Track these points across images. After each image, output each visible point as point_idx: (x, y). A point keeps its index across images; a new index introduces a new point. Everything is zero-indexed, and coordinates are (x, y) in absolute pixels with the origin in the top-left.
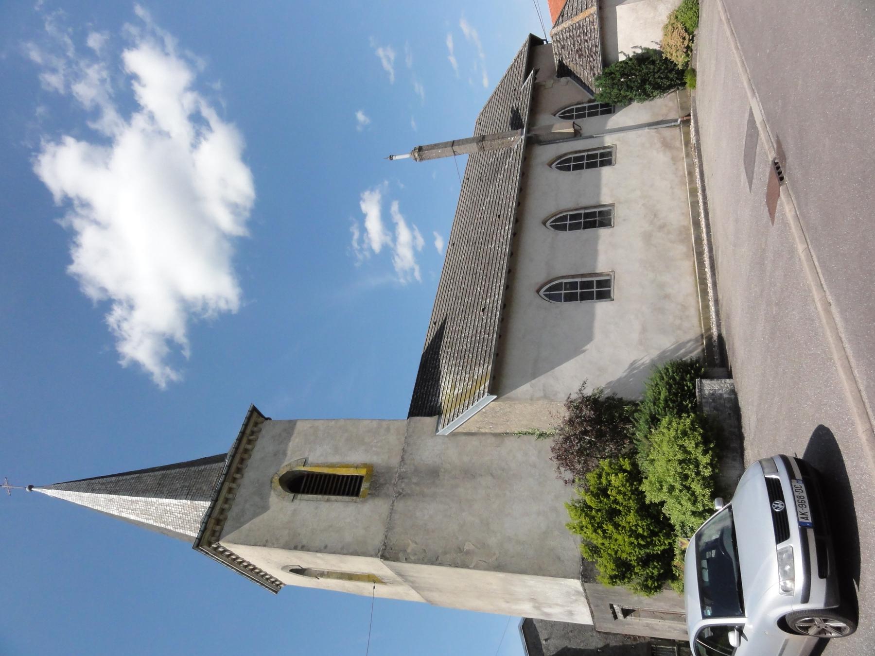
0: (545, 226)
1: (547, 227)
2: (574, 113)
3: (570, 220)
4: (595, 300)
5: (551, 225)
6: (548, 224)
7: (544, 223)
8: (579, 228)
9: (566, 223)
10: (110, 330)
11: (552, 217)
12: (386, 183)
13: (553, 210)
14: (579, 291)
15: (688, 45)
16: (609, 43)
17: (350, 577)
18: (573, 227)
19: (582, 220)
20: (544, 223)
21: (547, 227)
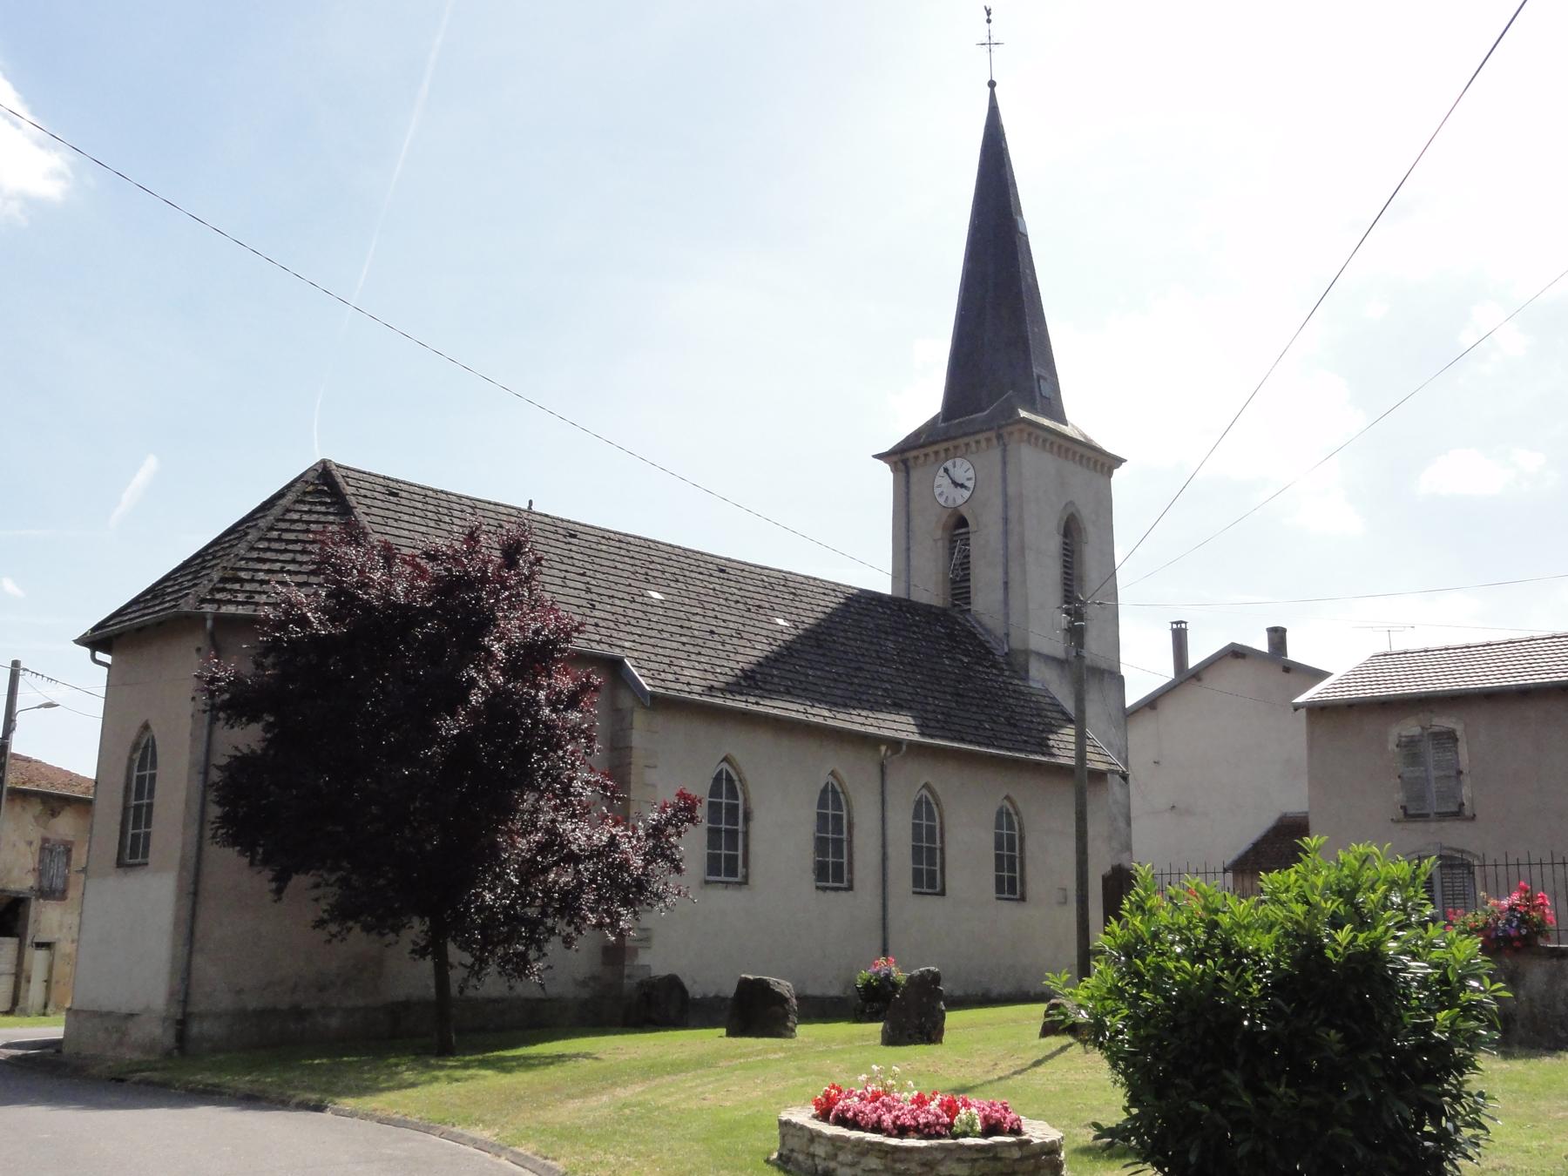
0: (722, 761)
1: (720, 763)
2: (924, 822)
3: (828, 809)
4: (995, 873)
5: (922, 795)
6: (725, 766)
7: (725, 759)
8: (914, 839)
9: (924, 819)
10: (247, 737)
11: (738, 774)
12: (227, 808)
13: (748, 776)
14: (724, 800)
15: (406, 1071)
16: (903, 483)
17: (774, 707)
18: (822, 818)
19: (924, 845)
20: (725, 759)
21: (720, 763)
